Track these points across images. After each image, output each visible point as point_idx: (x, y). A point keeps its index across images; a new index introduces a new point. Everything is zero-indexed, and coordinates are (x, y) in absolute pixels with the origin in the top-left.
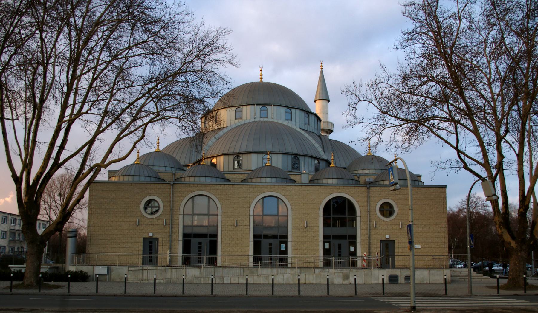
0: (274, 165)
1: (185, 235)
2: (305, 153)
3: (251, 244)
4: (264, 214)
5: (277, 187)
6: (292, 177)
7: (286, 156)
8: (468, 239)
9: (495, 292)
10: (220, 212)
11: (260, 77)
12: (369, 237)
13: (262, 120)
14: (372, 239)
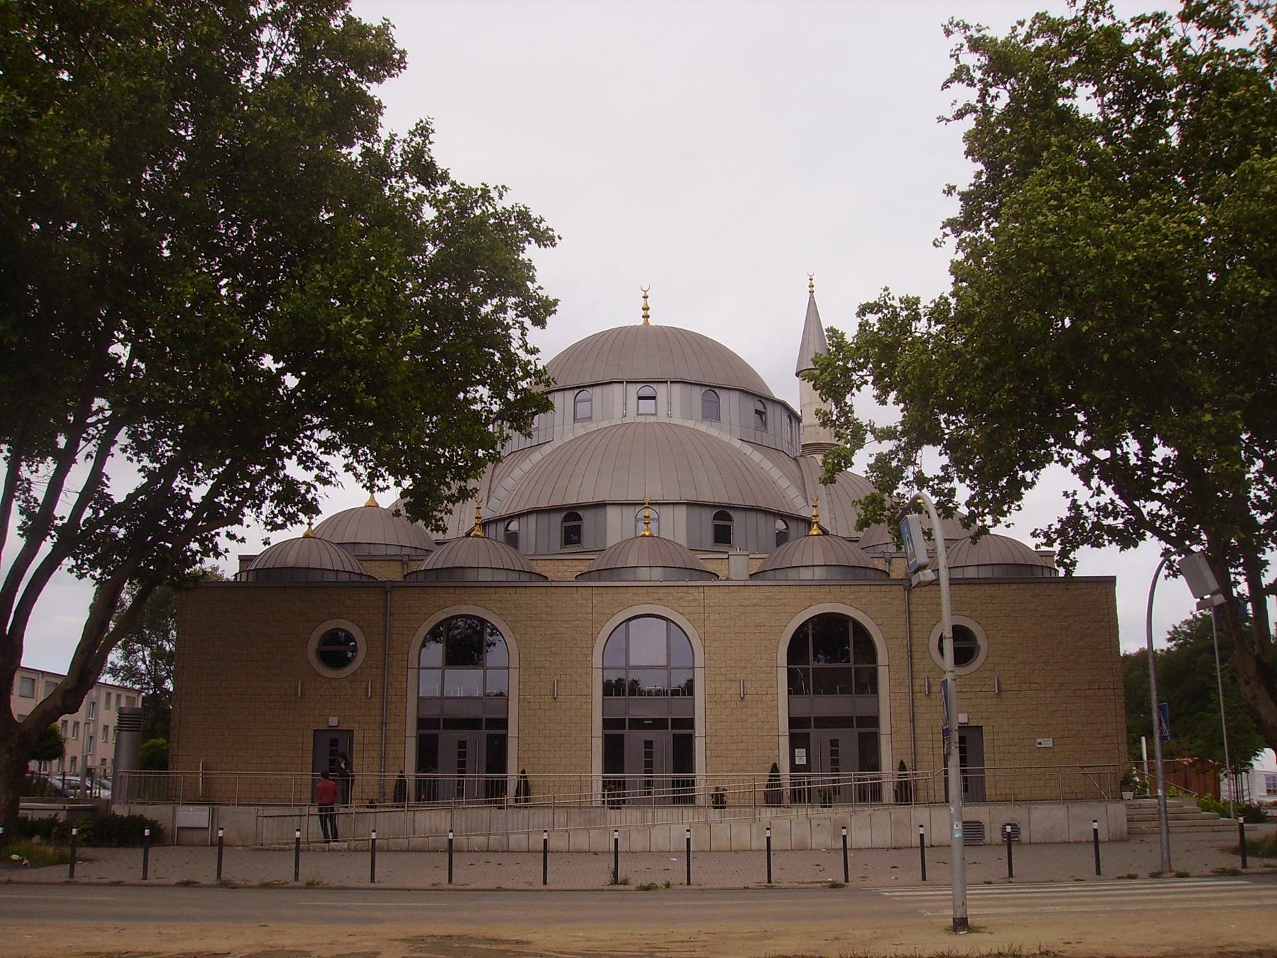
0: (666, 534)
1: (422, 723)
2: (750, 503)
3: (598, 744)
5: (665, 590)
6: (710, 567)
7: (697, 511)
8: (1155, 718)
9: (1235, 861)
10: (514, 661)
11: (643, 313)
12: (913, 720)
13: (642, 419)
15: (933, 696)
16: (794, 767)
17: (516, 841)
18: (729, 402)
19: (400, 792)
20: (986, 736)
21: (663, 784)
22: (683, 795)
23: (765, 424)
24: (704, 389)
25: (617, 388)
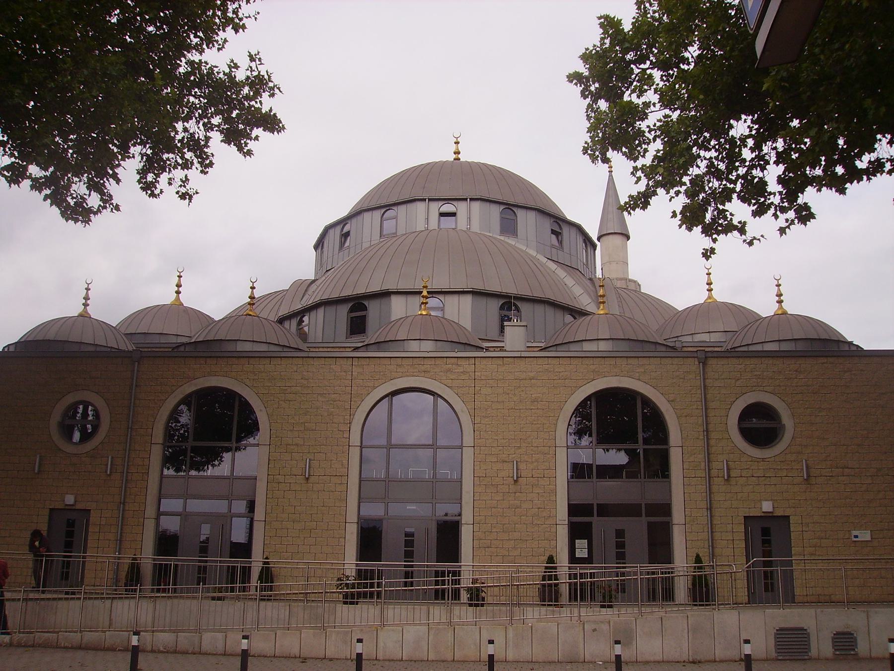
2: (538, 294)
4: (394, 441)
5: (433, 362)
7: (483, 301)
11: (455, 156)
12: (710, 509)
14: (717, 513)
15: (733, 481)
16: (573, 559)
17: (211, 640)
18: (526, 221)
19: (134, 576)
20: (795, 527)
21: (426, 574)
22: (444, 593)
23: (561, 243)
24: (502, 207)
25: (421, 207)
